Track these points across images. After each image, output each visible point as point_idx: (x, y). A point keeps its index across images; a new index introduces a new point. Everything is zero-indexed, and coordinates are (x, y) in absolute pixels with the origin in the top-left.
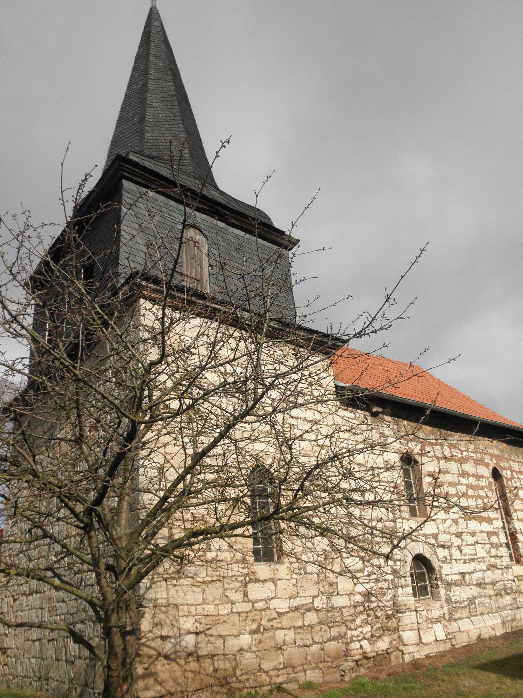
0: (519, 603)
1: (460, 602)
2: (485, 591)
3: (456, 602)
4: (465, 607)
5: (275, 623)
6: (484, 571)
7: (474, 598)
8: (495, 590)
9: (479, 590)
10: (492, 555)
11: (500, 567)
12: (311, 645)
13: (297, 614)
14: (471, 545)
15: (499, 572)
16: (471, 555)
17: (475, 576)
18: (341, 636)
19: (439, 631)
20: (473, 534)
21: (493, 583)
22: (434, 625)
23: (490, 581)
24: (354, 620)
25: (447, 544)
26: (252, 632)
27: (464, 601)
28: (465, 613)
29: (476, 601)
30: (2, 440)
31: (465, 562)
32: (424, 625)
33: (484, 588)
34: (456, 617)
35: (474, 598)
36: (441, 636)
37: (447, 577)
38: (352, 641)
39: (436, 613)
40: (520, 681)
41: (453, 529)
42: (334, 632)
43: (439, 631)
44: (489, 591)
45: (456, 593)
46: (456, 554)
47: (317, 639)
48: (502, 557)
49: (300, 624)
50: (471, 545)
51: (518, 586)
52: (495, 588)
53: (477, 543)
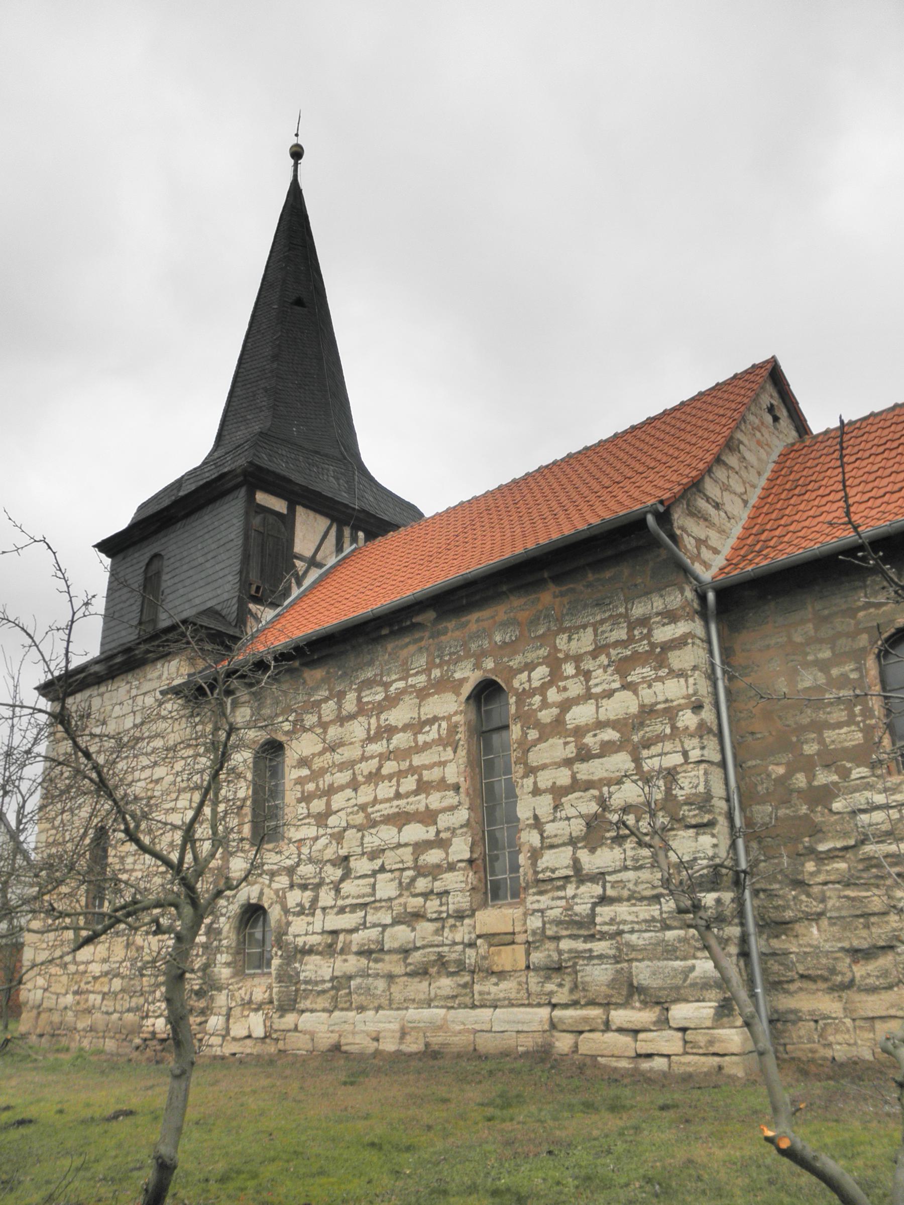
0: (476, 996)
1: (316, 983)
2: (379, 965)
3: (307, 982)
4: (324, 992)
5: (89, 987)
6: (385, 927)
7: (350, 978)
8: (407, 965)
9: (364, 961)
10: (418, 891)
11: (435, 916)
12: (112, 1013)
13: (105, 980)
14: (365, 876)
15: (430, 927)
16: (359, 897)
17: (358, 938)
18: (138, 1009)
19: (256, 1023)
20: (373, 855)
21: (406, 952)
22: (252, 1014)
23: (396, 945)
24: (154, 992)
25: (311, 881)
26: (76, 993)
27: (324, 981)
28: (323, 1002)
29: (352, 982)
30: (900, 911)
31: (342, 910)
32: (236, 1012)
33: (376, 961)
34: (301, 1006)
35: (350, 978)
36: (259, 1032)
37: (297, 939)
38: (147, 1016)
39: (259, 995)
40: (141, 1199)
41: (329, 854)
42: (135, 1002)
43: (256, 1023)
44: (392, 964)
45: (308, 967)
46: (326, 897)
47: (118, 1008)
48: (447, 892)
49: (106, 989)
50: (365, 876)
51: (484, 958)
52: (409, 961)
53: (382, 869)
